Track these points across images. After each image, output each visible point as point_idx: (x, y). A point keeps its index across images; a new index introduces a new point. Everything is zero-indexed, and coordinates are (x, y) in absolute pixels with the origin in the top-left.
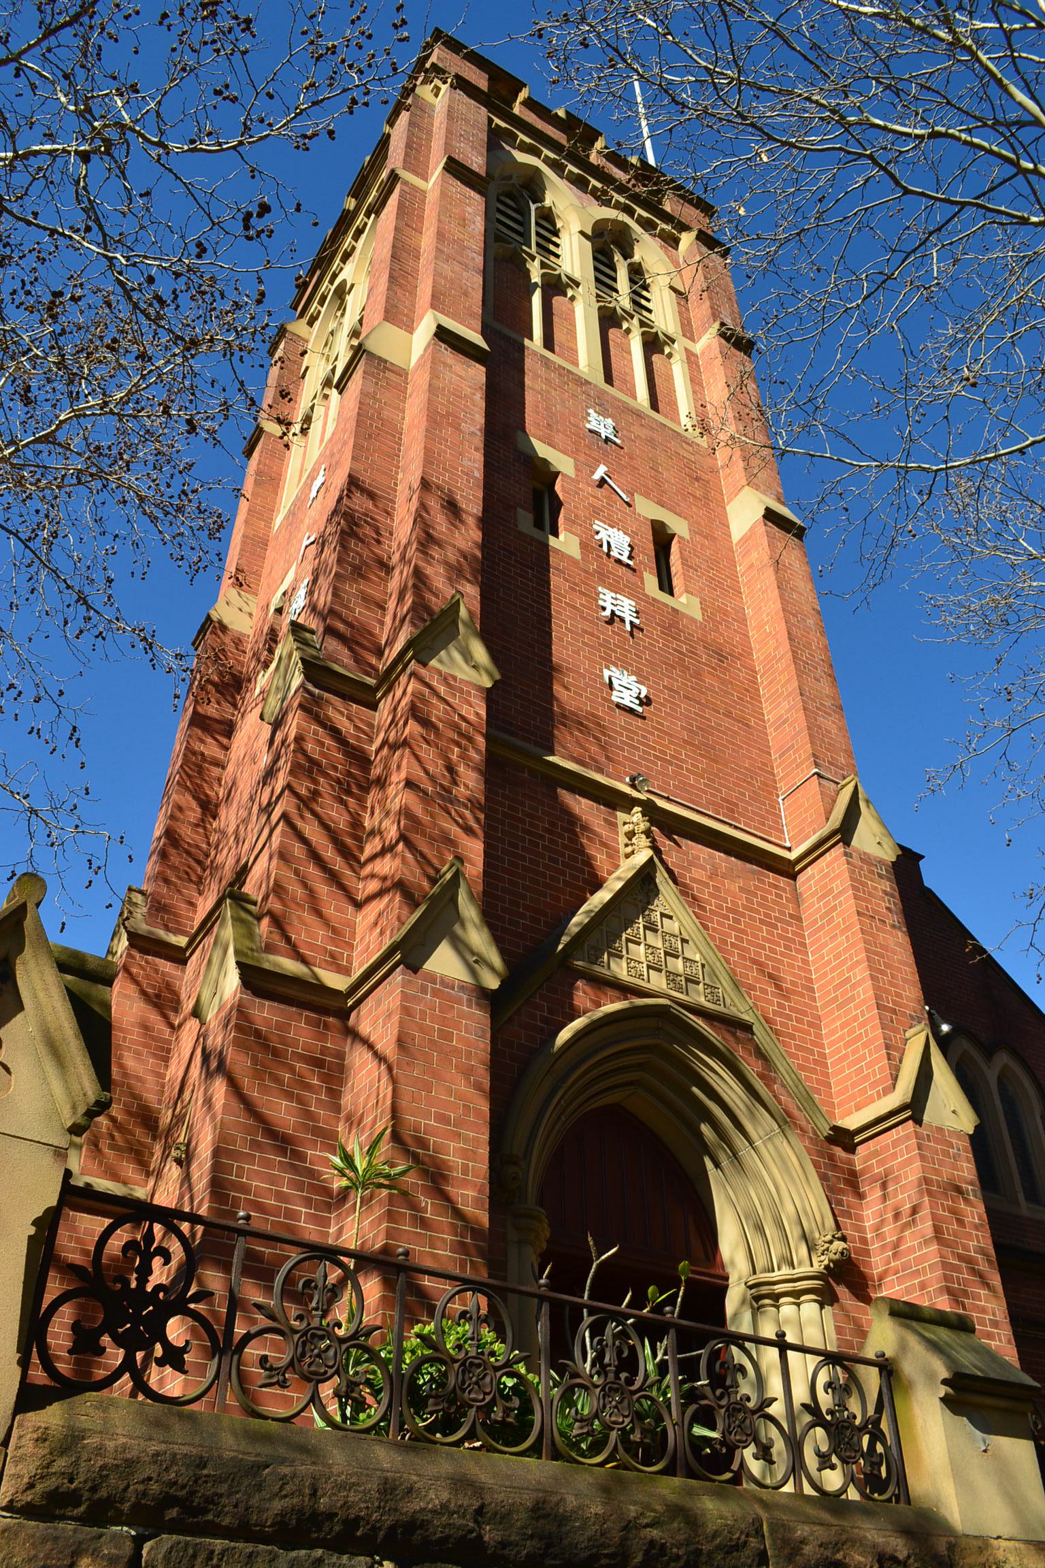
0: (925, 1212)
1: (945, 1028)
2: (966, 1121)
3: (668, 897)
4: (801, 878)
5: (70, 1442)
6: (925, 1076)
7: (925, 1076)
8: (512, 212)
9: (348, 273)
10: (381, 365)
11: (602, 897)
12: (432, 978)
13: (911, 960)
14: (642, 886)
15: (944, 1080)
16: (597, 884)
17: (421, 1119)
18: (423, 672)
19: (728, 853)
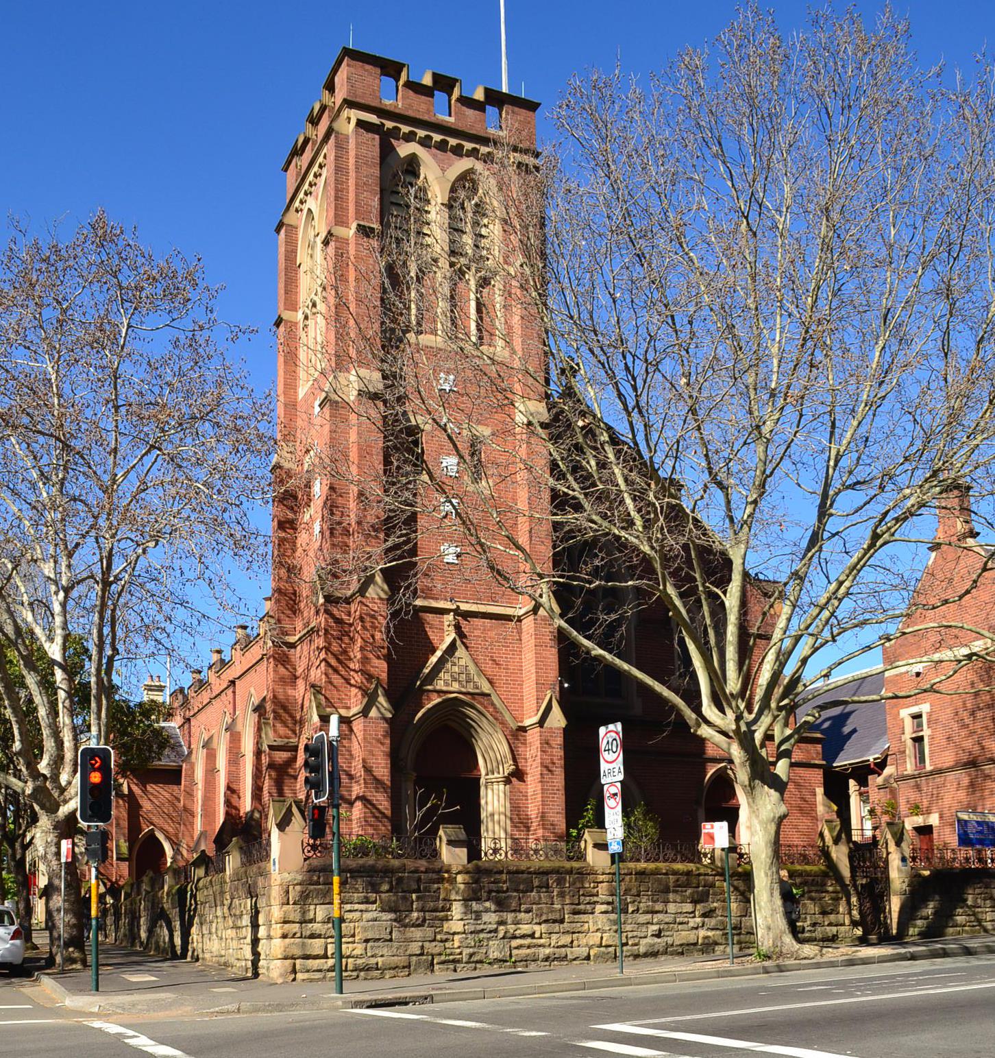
0: (539, 757)
1: (566, 685)
2: (562, 723)
3: (461, 652)
4: (523, 622)
5: (310, 864)
6: (549, 708)
7: (549, 708)
8: (396, 179)
9: (311, 203)
10: (338, 239)
11: (439, 653)
12: (372, 718)
13: (557, 660)
14: (452, 648)
15: (556, 710)
16: (434, 651)
17: (371, 762)
18: (364, 600)
19: (491, 619)
